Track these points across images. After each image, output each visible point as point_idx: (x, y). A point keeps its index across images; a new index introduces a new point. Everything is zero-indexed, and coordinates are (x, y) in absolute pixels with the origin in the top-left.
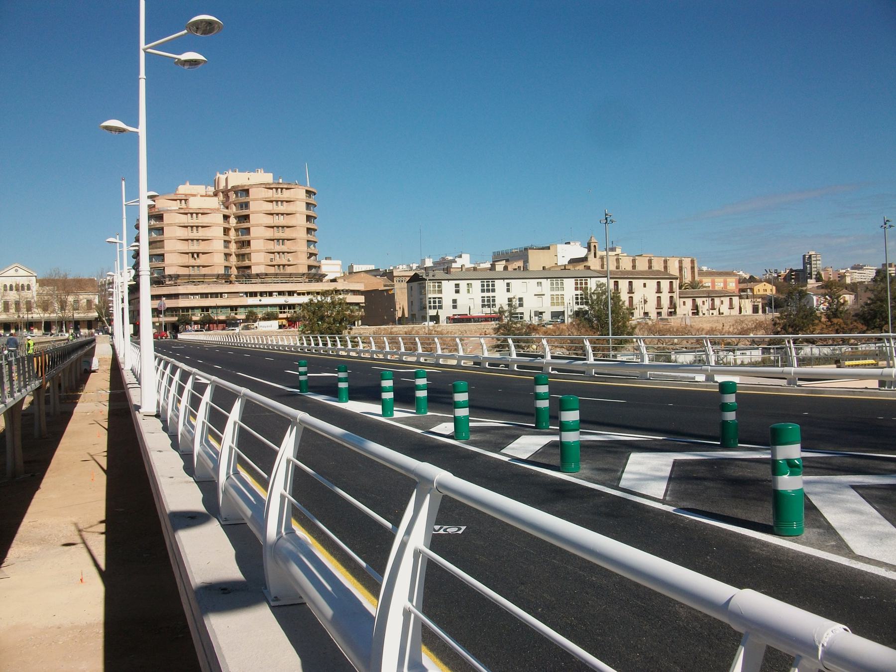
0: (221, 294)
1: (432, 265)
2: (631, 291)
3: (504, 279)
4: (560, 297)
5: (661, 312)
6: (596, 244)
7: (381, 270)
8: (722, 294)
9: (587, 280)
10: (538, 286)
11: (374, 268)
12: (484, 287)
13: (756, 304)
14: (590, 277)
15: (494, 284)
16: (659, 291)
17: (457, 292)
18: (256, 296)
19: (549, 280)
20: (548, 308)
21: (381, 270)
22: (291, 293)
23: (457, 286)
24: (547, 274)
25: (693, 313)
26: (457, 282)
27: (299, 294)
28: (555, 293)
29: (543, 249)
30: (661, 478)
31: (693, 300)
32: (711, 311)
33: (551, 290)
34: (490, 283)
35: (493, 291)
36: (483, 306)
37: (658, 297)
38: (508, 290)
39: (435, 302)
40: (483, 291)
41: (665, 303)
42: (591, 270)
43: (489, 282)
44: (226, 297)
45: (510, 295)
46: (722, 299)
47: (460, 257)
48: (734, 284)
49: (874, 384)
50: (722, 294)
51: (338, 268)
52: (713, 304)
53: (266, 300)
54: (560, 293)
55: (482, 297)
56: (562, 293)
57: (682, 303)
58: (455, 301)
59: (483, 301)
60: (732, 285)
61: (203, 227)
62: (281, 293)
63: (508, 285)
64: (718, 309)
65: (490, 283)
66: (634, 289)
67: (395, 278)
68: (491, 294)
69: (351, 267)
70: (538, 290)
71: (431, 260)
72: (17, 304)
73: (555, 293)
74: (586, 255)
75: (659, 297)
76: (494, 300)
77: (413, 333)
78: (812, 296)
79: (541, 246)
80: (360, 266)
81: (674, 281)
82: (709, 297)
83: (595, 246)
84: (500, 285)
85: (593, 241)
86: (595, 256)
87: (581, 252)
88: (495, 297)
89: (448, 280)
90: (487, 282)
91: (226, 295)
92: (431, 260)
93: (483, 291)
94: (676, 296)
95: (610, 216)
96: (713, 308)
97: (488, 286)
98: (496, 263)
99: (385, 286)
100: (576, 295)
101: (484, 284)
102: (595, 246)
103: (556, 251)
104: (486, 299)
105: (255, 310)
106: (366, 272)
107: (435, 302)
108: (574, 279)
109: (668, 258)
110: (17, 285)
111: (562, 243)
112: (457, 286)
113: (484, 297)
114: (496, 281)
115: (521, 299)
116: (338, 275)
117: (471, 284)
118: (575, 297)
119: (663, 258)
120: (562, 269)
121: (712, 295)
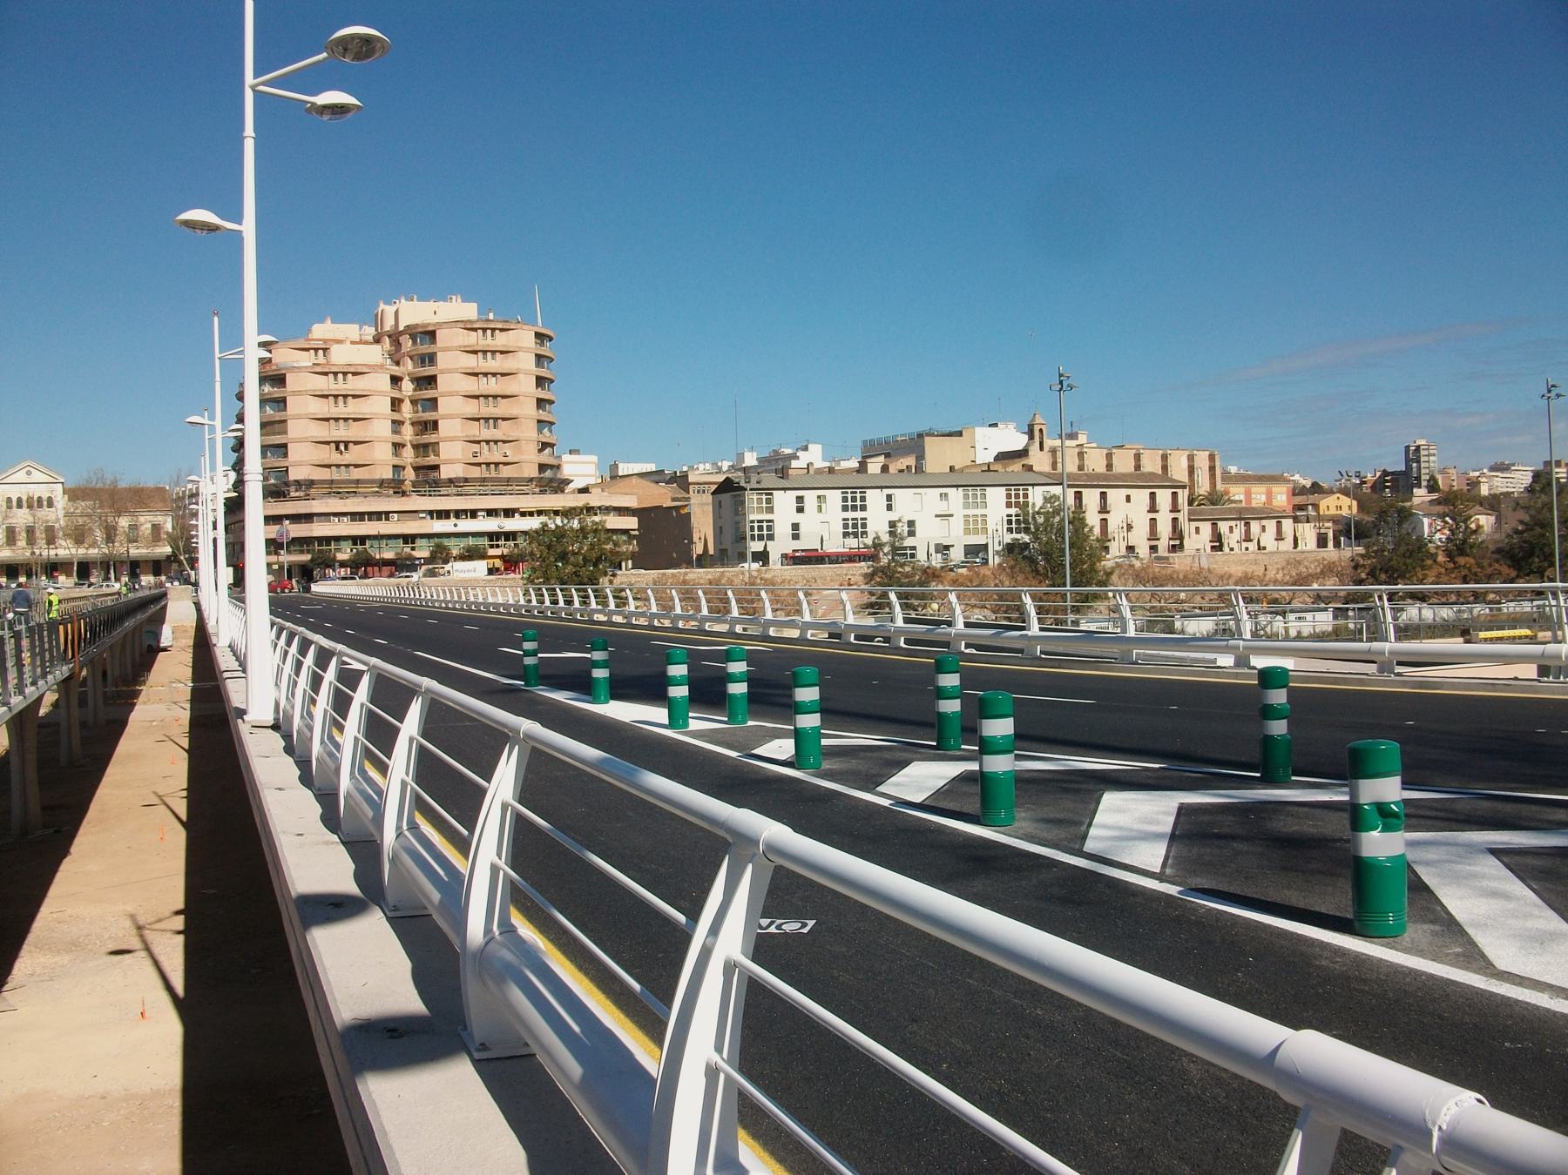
0: (387, 513)
1: (756, 463)
2: (1104, 509)
3: (881, 488)
4: (979, 519)
5: (1157, 546)
8: (1263, 514)
9: (1027, 490)
10: (941, 500)
11: (654, 469)
12: (847, 502)
13: (1322, 531)
14: (1033, 485)
15: (865, 497)
16: (1153, 508)
17: (800, 510)
18: (448, 517)
19: (960, 489)
20: (959, 539)
21: (666, 472)
22: (509, 513)
23: (800, 499)
24: (957, 479)
25: (1213, 548)
26: (800, 493)
27: (523, 514)
28: (971, 512)
29: (950, 435)
30: (1157, 836)
31: (1213, 524)
32: (1245, 545)
33: (964, 508)
34: (858, 495)
35: (863, 508)
36: (846, 535)
37: (1151, 519)
38: (889, 508)
39: (761, 529)
40: (845, 508)
41: (1164, 529)
42: (1034, 472)
43: (856, 493)
44: (396, 519)
45: (893, 516)
46: (1264, 522)
47: (806, 449)
48: (1284, 497)
50: (1263, 514)
51: (592, 469)
52: (1248, 532)
53: (466, 525)
54: (979, 512)
55: (844, 520)
56: (983, 512)
57: (1193, 530)
58: (795, 526)
59: (846, 526)
60: (1281, 498)
61: (355, 397)
62: (491, 513)
63: (889, 497)
64: (1256, 540)
65: (858, 495)
66: (1110, 505)
67: (691, 487)
68: (859, 514)
69: (614, 467)
70: (942, 508)
71: (755, 454)
72: (30, 531)
73: (971, 512)
74: (1026, 446)
75: (1153, 520)
76: (864, 525)
77: (723, 582)
78: (1421, 517)
79: (947, 430)
80: (631, 465)
81: (1180, 491)
82: (1240, 519)
83: (1041, 431)
84: (875, 498)
85: (1037, 421)
86: (1042, 448)
87: (1018, 441)
88: (865, 519)
89: (785, 489)
90: (852, 493)
91: (395, 515)
92: (755, 454)
93: (845, 508)
94: (1182, 517)
95: (1068, 377)
96: (1248, 539)
97: (854, 499)
98: (868, 460)
99: (674, 500)
100: (1008, 516)
101: (847, 497)
102: (1041, 431)
103: (973, 438)
104: (850, 522)
105: (446, 542)
106: (641, 475)
107: (761, 529)
108: (1004, 488)
109: (1169, 452)
110: (30, 499)
111: (983, 425)
112: (800, 499)
113: (848, 519)
114: (868, 491)
115: (911, 524)
116: (592, 481)
117: (824, 497)
118: (1005, 519)
119: (1161, 452)
120: (983, 471)
121: (1245, 516)
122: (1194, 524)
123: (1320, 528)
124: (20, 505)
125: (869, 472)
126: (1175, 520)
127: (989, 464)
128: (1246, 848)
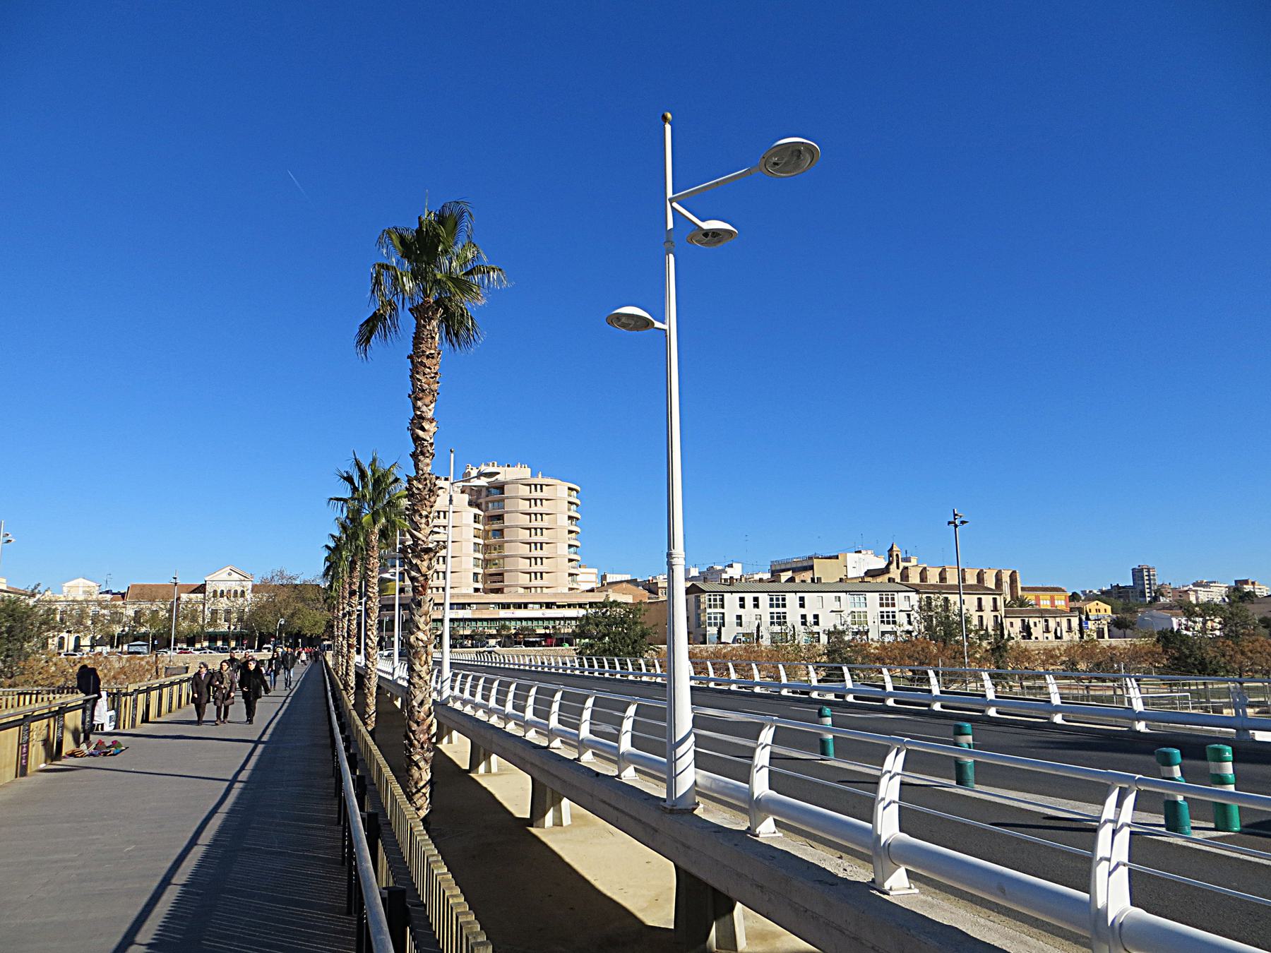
0: (469, 604)
1: (697, 575)
3: (796, 592)
4: (862, 614)
6: (899, 553)
7: (638, 580)
8: (1056, 613)
10: (836, 601)
11: (629, 579)
12: (773, 601)
13: (1100, 626)
14: (898, 592)
16: (980, 608)
17: (742, 606)
18: (509, 608)
21: (638, 580)
23: (742, 599)
24: (844, 586)
25: (1024, 637)
26: (802, 595)
27: (559, 607)
29: (830, 558)
32: (1046, 635)
33: (770, 607)
34: (890, 597)
35: (784, 606)
38: (802, 606)
39: (888, 617)
44: (475, 608)
45: (803, 611)
46: (1058, 620)
47: (731, 566)
48: (1063, 603)
49: (473, 656)
50: (1056, 613)
51: (593, 578)
52: (1047, 627)
57: (1009, 625)
58: (739, 617)
59: (772, 618)
60: (1061, 603)
63: (802, 599)
64: (1054, 631)
65: (890, 597)
67: (660, 590)
68: (781, 610)
69: (604, 577)
70: (836, 607)
71: (697, 569)
72: (228, 612)
76: (785, 617)
77: (367, 641)
79: (828, 555)
80: (615, 576)
81: (998, 597)
82: (1042, 617)
83: (897, 555)
84: (793, 600)
86: (898, 568)
87: (881, 563)
88: (785, 613)
89: (732, 592)
90: (891, 595)
91: (475, 606)
92: (697, 569)
95: (961, 516)
96: (1047, 630)
97: (887, 599)
98: (781, 574)
99: (649, 599)
100: (881, 612)
102: (897, 555)
103: (846, 560)
106: (628, 581)
107: (888, 617)
108: (878, 594)
110: (229, 591)
111: (852, 552)
112: (742, 599)
114: (787, 594)
115: (816, 617)
116: (594, 585)
117: (909, 597)
118: (880, 614)
121: (1043, 614)
122: (1009, 620)
123: (1099, 624)
124: (222, 595)
125: (823, 582)
126: (996, 617)
127: (863, 578)
128: (1073, 865)
